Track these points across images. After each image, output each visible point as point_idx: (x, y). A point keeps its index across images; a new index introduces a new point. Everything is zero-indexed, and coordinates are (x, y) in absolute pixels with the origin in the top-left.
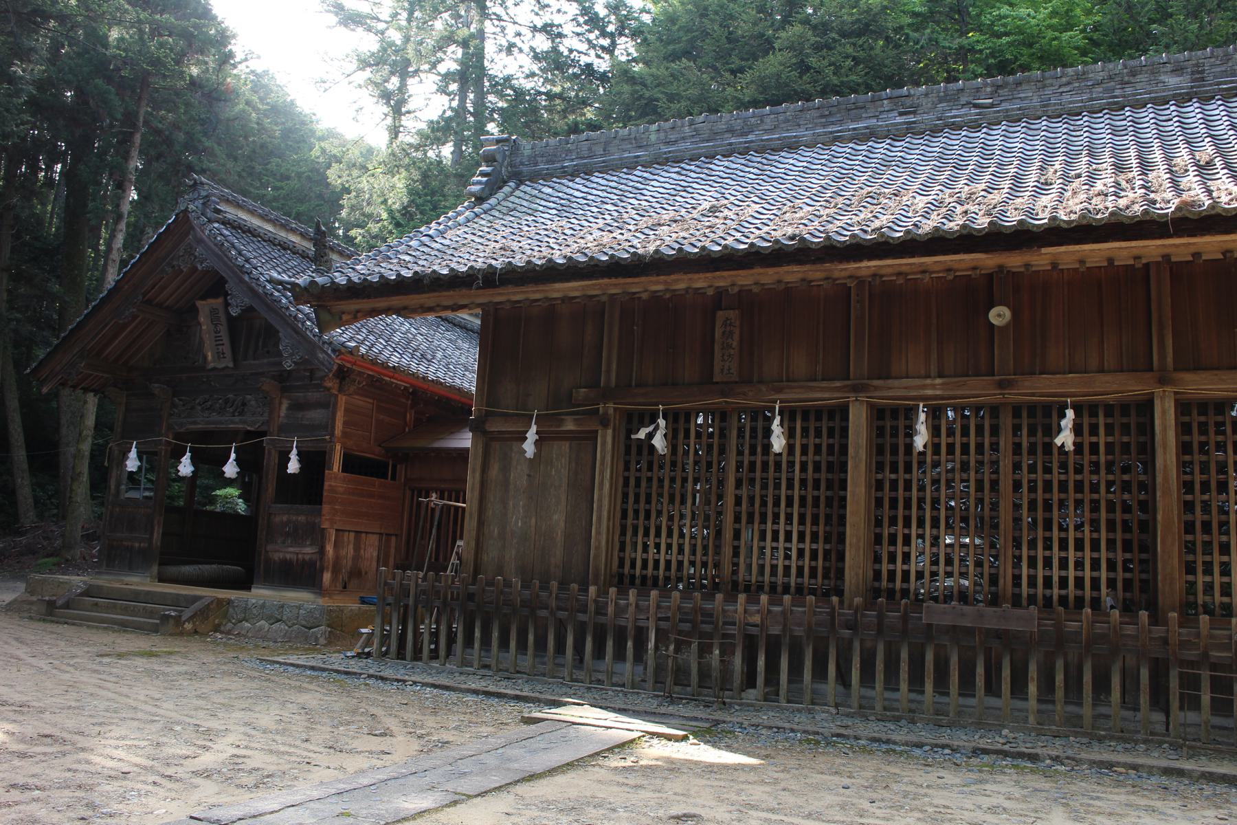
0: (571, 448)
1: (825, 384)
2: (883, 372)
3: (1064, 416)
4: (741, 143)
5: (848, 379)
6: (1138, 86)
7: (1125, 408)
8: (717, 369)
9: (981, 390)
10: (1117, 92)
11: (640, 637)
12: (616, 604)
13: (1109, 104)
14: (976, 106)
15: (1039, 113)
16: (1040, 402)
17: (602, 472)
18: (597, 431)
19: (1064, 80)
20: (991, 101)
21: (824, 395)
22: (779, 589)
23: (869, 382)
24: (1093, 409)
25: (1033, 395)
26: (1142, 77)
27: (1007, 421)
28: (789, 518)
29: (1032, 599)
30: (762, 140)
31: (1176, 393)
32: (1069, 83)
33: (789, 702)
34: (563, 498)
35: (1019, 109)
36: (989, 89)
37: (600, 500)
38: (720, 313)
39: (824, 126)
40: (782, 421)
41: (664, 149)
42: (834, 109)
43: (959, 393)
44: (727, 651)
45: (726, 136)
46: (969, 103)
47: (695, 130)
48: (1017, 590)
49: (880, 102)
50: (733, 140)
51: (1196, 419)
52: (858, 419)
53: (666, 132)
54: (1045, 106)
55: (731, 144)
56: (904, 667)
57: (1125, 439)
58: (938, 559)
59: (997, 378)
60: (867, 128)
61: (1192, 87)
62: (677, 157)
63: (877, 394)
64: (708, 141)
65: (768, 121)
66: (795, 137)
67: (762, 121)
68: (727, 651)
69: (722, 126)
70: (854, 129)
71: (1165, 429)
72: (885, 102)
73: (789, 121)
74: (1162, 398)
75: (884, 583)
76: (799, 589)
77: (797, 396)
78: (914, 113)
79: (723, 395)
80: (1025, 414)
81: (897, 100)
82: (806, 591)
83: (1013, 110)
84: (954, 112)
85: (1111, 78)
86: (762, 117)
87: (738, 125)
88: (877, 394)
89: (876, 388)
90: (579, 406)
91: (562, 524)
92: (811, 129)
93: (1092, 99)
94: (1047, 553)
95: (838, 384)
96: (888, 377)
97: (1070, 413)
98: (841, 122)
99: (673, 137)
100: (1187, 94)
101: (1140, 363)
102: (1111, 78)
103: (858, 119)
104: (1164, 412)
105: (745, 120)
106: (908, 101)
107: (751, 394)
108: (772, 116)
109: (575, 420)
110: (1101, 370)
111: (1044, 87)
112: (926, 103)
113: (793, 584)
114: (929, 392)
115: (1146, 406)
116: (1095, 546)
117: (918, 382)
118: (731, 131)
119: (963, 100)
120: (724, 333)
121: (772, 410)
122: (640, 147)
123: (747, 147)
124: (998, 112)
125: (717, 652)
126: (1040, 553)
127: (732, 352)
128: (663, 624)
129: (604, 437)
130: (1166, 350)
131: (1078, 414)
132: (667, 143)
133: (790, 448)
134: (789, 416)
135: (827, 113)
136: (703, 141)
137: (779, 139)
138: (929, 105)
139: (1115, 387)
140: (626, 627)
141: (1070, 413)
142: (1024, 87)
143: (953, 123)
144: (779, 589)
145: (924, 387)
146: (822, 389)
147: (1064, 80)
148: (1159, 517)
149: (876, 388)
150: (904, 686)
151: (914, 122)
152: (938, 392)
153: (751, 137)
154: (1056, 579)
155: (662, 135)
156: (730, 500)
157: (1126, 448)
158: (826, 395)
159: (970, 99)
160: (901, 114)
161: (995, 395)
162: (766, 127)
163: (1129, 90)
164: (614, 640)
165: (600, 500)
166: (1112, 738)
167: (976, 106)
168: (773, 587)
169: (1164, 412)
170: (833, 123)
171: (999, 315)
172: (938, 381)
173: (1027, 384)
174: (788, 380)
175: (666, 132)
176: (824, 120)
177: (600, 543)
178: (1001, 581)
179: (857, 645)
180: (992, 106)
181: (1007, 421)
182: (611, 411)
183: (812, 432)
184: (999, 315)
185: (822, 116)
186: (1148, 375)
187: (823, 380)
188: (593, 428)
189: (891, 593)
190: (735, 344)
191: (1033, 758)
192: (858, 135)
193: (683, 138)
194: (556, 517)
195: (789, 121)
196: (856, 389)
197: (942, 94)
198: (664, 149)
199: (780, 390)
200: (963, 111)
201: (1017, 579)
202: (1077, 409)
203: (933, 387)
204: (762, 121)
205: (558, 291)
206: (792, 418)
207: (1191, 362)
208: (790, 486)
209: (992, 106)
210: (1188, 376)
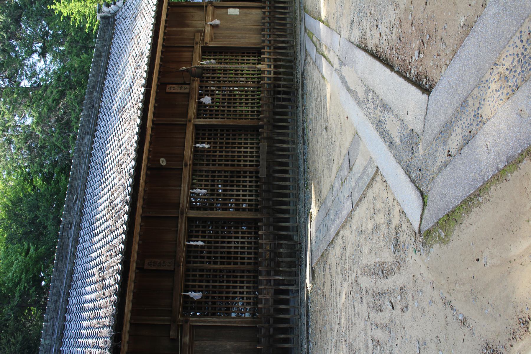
0: (197, 340)
1: (179, 225)
2: (177, 205)
3: (198, 147)
4: (63, 297)
5: (178, 217)
6: (85, 149)
7: (197, 134)
8: (168, 268)
9: (187, 173)
10: (85, 156)
11: (278, 283)
12: (265, 294)
13: (88, 157)
14: (76, 201)
15: (85, 179)
16: (186, 249)
17: (209, 322)
18: (190, 325)
19: (75, 171)
20: (75, 196)
21: (183, 225)
22: (256, 246)
23: (180, 209)
24: (197, 138)
25: (190, 157)
26: (82, 148)
27: (198, 167)
28: (229, 242)
29: (257, 161)
30: (65, 287)
31: (194, 118)
32: (77, 170)
33: (297, 222)
34: (220, 343)
35: (82, 186)
36: (71, 196)
37: (221, 322)
38: (145, 267)
39: (67, 260)
40: (192, 241)
41: (55, 336)
42: (61, 255)
43: (187, 179)
44: (280, 246)
45: (58, 305)
46: (74, 204)
47: (51, 320)
48: (254, 166)
49: (63, 237)
50: (61, 301)
51: (194, 233)
52: (193, 214)
53: (46, 335)
54: (83, 178)
55: (63, 301)
56: (281, 191)
57: (207, 134)
58: (241, 297)
59: (184, 167)
60: (72, 242)
61: (90, 134)
62: (61, 329)
63: (185, 206)
64: (58, 313)
65: (57, 284)
66: (68, 272)
67: (56, 287)
68: (280, 246)
69: (52, 306)
70: (72, 247)
71: (205, 122)
72: (64, 234)
73: (60, 275)
74: (195, 122)
75: (253, 207)
76: (256, 238)
77: (183, 235)
78: (71, 224)
79: (179, 266)
80: (190, 259)
81: (64, 230)
82: (256, 261)
83: (81, 188)
84: (76, 209)
85: (79, 157)
86: (54, 287)
87: (54, 298)
88: (185, 206)
89: (183, 206)
90: (178, 337)
91: (232, 343)
92: (66, 265)
93: (85, 163)
94: (239, 258)
95: (180, 220)
96: (179, 203)
97: (198, 145)
98: (67, 253)
99: (51, 331)
100: (92, 136)
101: (184, 127)
102: (79, 157)
103: (67, 246)
104: (200, 121)
105: (53, 294)
106: (66, 225)
107: (180, 254)
108: (55, 282)
109: (184, 337)
110: (185, 138)
111: (75, 178)
112: (69, 219)
113: (254, 240)
114: (186, 188)
115: (191, 220)
116: (238, 191)
117: (182, 192)
118: (56, 302)
119: (72, 205)
120: (154, 265)
121: (184, 295)
122: (50, 349)
123: (67, 293)
124: (80, 193)
125: (281, 250)
126: (241, 193)
127: (162, 262)
128: (272, 273)
129: (193, 321)
130: (180, 120)
131: (198, 143)
132: (53, 334)
133: (208, 143)
134: (190, 238)
135: (61, 258)
136: (57, 316)
137: (67, 279)
138: (70, 218)
139: (191, 133)
140: (275, 289)
141: (198, 145)
142: (73, 184)
143: (80, 209)
144: (256, 246)
145: (184, 190)
146: (181, 226)
147: (75, 171)
148: (232, 124)
149: (183, 206)
150: (288, 183)
151: (76, 223)
152: (187, 185)
153: (62, 293)
154: (250, 154)
155: (48, 337)
156: (222, 266)
157: (209, 135)
158: (184, 224)
159: (72, 203)
160: (71, 228)
161: (189, 168)
162: (60, 285)
163: (86, 152)
164: (280, 305)
165: (221, 322)
166: (297, 125)
167: (76, 201)
168: (254, 282)
169: (200, 121)
170: (66, 256)
171: (163, 162)
172: (182, 185)
173: (186, 158)
174: (176, 241)
175: (46, 335)
176: (64, 260)
177: (239, 322)
178: (252, 170)
179: (275, 199)
180: (77, 196)
181: (198, 167)
182: (182, 318)
183: (197, 234)
184: (163, 162)
185: (62, 260)
186: (188, 125)
187: (177, 227)
188: (189, 326)
189: (257, 205)
190: (159, 261)
191: (304, 129)
192: (74, 245)
193: (53, 326)
194: (228, 347)
195: (60, 275)
196: (182, 214)
197: (67, 213)
198: (55, 336)
199: (180, 243)
200: (76, 206)
201: (251, 166)
202: (196, 143)
203: (184, 187)
204: (56, 287)
205: (133, 264)
206: (191, 237)
207: (185, 114)
208: (217, 242)
209: (77, 196)
210: (189, 115)
